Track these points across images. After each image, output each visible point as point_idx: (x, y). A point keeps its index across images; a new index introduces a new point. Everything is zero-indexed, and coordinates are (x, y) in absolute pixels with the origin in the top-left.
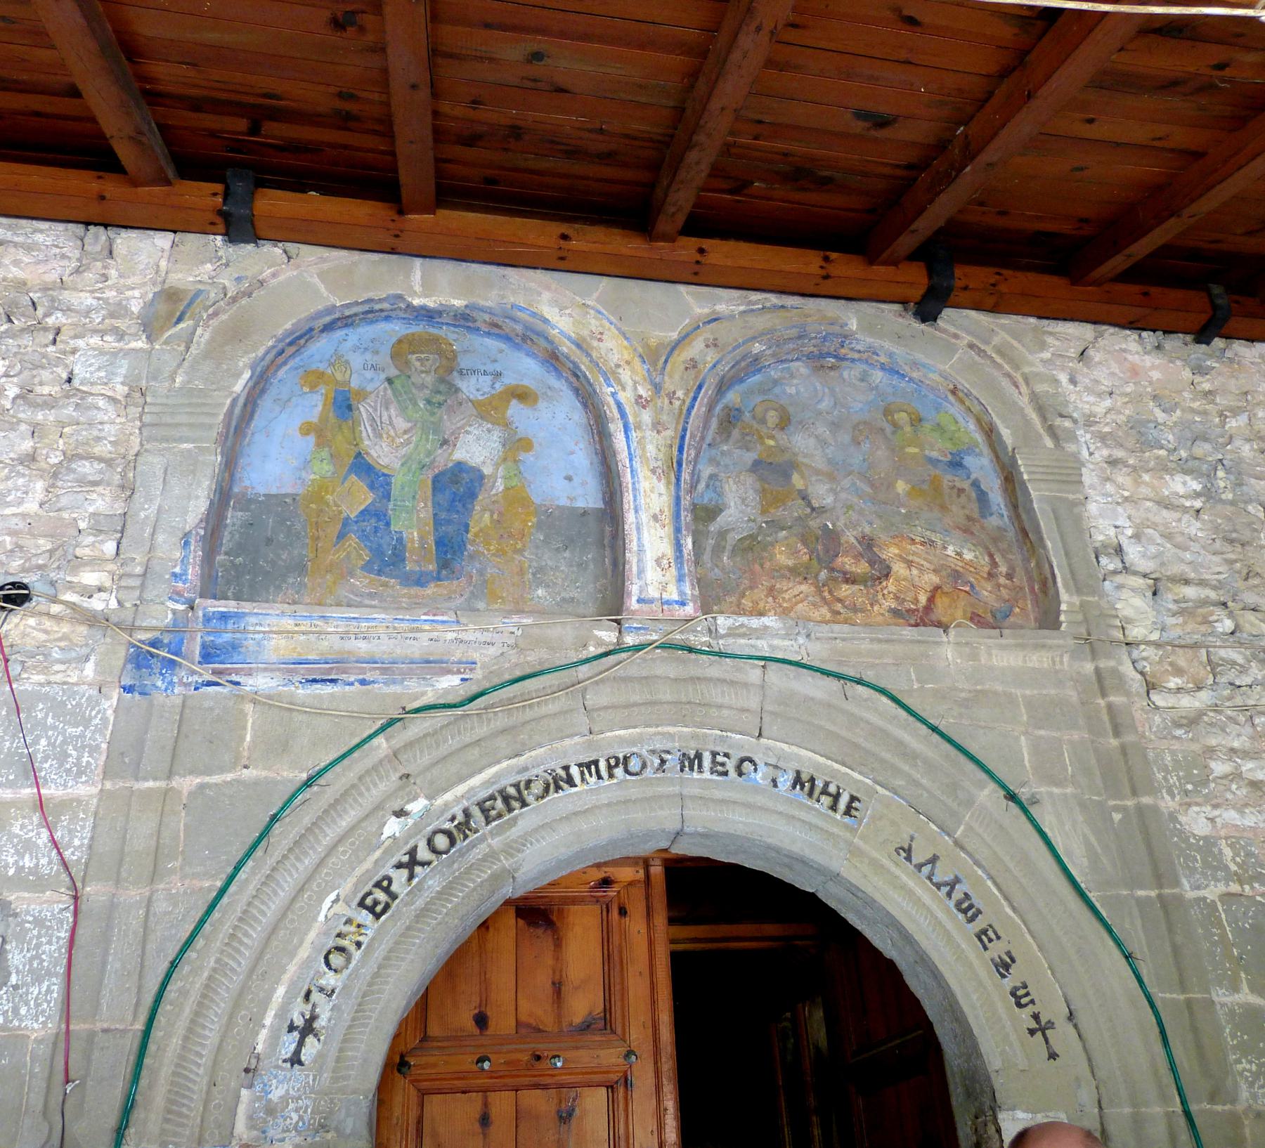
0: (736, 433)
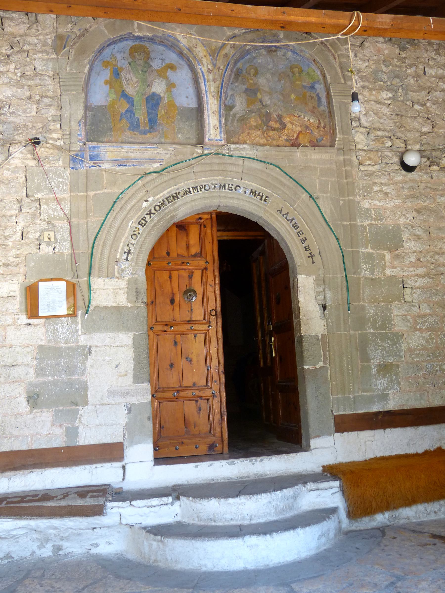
0: (240, 78)
